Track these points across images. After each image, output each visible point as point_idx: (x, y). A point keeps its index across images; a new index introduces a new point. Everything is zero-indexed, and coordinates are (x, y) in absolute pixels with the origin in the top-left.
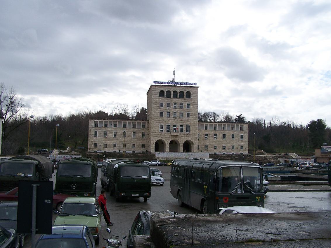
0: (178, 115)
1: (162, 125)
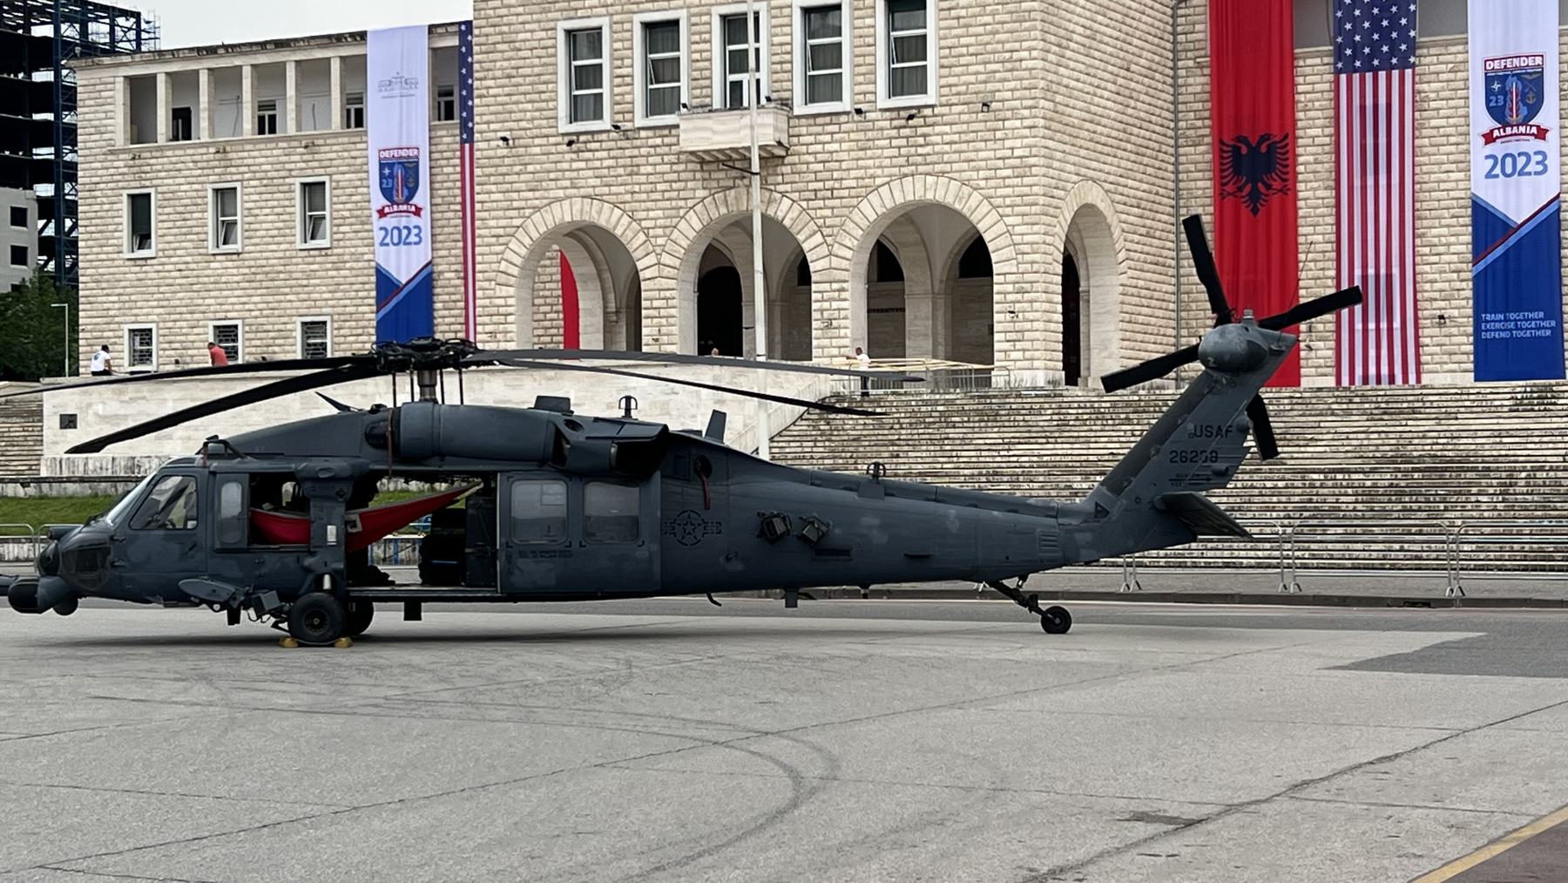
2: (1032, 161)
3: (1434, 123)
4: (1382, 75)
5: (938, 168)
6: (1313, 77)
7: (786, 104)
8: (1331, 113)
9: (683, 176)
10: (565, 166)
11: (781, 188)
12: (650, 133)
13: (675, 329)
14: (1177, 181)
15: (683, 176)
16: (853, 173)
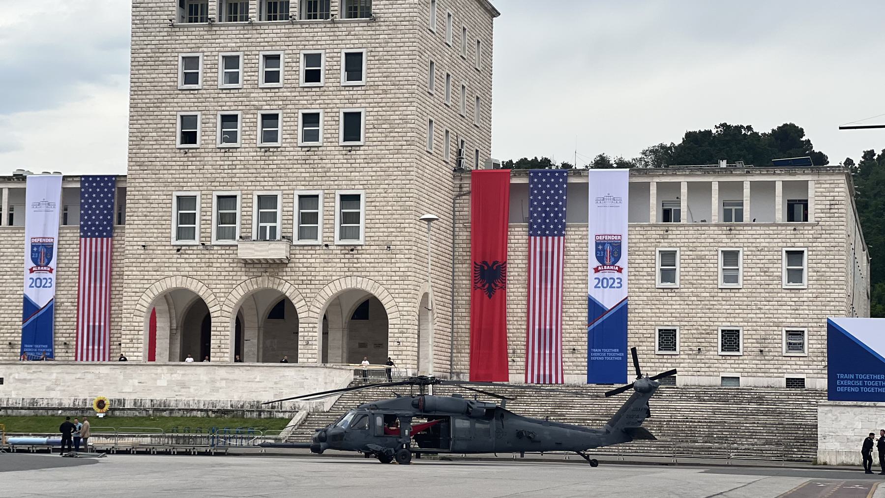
0: (290, 128)
1: (185, 202)
2: (409, 274)
3: (572, 261)
4: (550, 238)
5: (363, 274)
6: (518, 237)
7: (290, 239)
8: (527, 253)
9: (235, 269)
10: (174, 260)
11: (285, 278)
12: (219, 248)
13: (228, 342)
14: (453, 280)
15: (235, 269)
16: (322, 274)
